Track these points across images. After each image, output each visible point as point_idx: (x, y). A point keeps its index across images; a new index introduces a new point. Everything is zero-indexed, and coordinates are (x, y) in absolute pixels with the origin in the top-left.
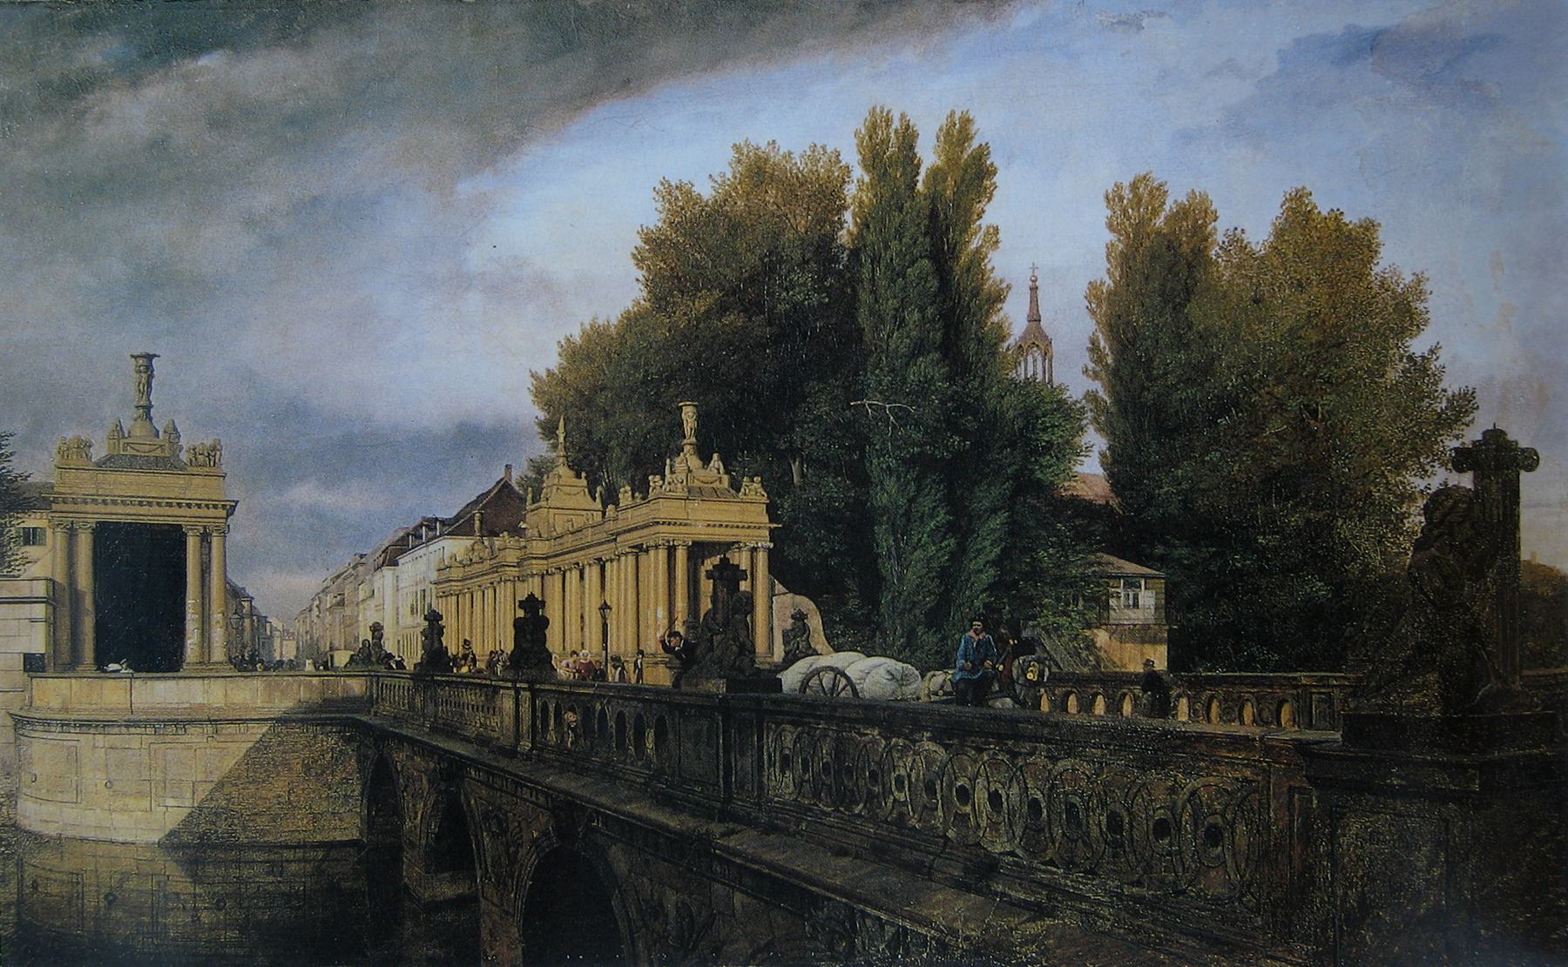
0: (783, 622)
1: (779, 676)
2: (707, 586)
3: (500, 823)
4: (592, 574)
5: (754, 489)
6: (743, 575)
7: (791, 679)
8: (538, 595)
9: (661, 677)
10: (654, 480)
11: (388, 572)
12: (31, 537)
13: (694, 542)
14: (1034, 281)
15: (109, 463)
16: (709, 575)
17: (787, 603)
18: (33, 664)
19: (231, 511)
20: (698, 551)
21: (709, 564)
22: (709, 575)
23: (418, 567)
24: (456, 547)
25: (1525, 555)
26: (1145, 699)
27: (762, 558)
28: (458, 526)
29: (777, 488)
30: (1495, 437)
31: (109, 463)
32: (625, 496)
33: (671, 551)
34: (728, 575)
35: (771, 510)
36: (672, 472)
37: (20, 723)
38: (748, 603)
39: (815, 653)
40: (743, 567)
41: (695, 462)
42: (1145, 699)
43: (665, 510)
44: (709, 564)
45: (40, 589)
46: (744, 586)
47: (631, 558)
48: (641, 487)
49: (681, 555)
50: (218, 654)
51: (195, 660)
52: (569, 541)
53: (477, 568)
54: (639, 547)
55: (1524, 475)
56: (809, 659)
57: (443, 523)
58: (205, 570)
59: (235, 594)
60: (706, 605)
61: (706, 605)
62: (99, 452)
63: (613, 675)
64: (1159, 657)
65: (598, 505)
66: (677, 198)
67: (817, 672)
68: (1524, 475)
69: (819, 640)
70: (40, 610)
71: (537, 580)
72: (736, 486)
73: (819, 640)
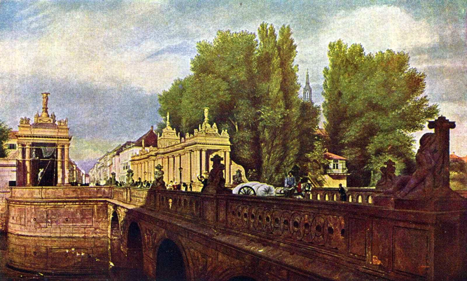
0: (234, 173)
1: (232, 189)
2: (211, 163)
3: (150, 231)
4: (177, 159)
5: (225, 133)
6: (222, 159)
7: (235, 191)
8: (161, 165)
9: (198, 188)
10: (196, 131)
11: (117, 157)
12: (12, 147)
13: (208, 149)
14: (308, 73)
15: (36, 125)
16: (212, 160)
17: (236, 167)
18: (12, 184)
19: (70, 139)
20: (209, 152)
21: (211, 157)
22: (212, 160)
23: (128, 155)
24: (137, 150)
25: (451, 153)
26: (339, 195)
27: (228, 154)
28: (138, 144)
29: (231, 132)
30: (442, 119)
31: (36, 125)
32: (187, 136)
33: (201, 151)
34: (217, 160)
35: (231, 140)
36: (201, 128)
37: (8, 201)
38: (223, 167)
39: (243, 182)
40: (222, 157)
41: (209, 126)
42: (339, 195)
43: (199, 139)
44: (211, 157)
45: (14, 163)
46: (222, 162)
47: (189, 154)
48: (192, 132)
49: (204, 153)
50: (66, 181)
51: (61, 183)
52: (170, 149)
53: (143, 157)
54: (191, 151)
55: (451, 130)
56: (241, 184)
57: (133, 143)
58: (63, 158)
59: (70, 163)
60: (211, 168)
61: (211, 168)
62: (32, 121)
63: (183, 189)
64: (344, 183)
65: (179, 138)
66: (204, 48)
67: (243, 188)
68: (451, 130)
69: (244, 178)
70: (15, 168)
71: (161, 160)
72: (220, 132)
73: (244, 178)
